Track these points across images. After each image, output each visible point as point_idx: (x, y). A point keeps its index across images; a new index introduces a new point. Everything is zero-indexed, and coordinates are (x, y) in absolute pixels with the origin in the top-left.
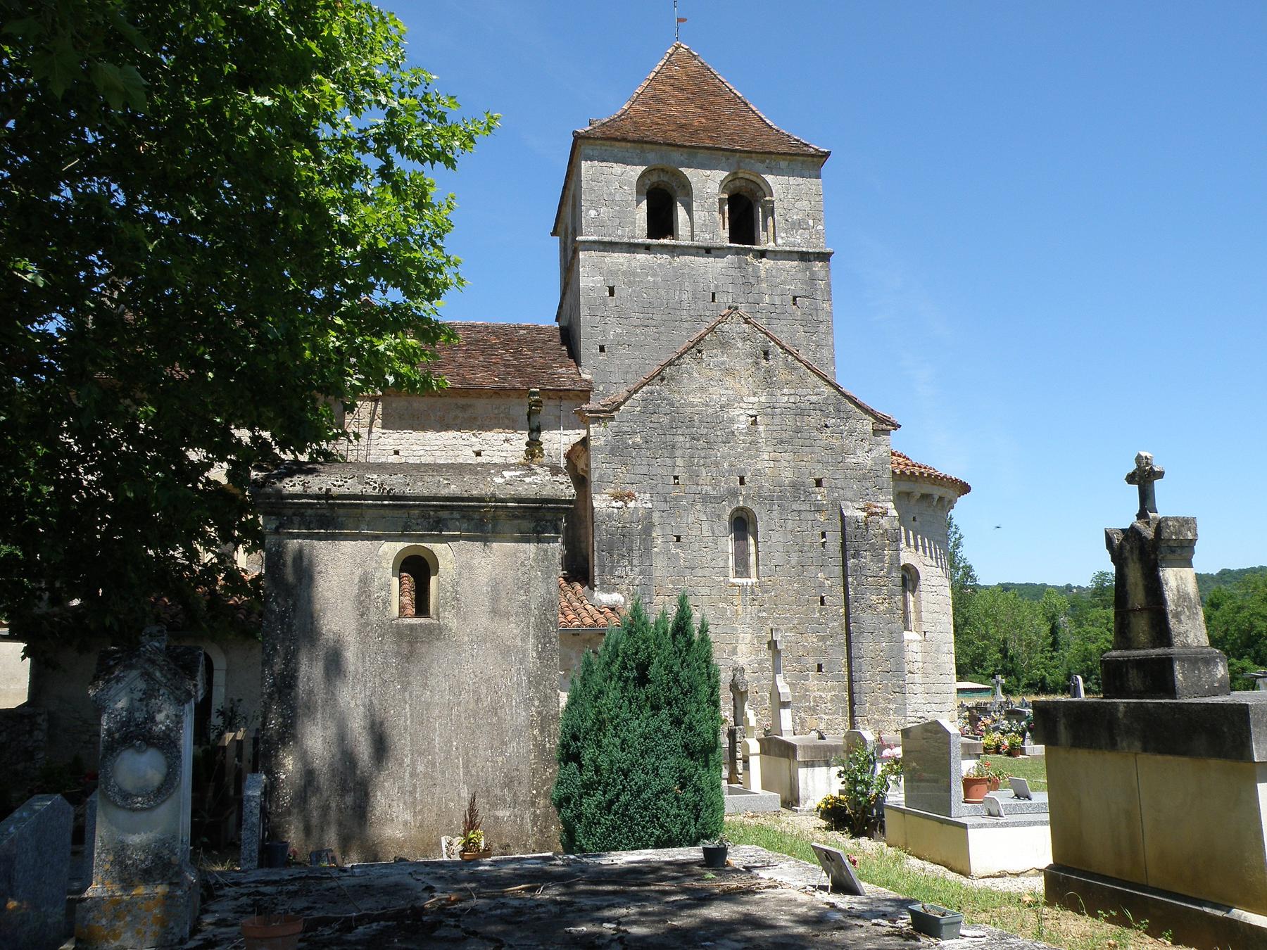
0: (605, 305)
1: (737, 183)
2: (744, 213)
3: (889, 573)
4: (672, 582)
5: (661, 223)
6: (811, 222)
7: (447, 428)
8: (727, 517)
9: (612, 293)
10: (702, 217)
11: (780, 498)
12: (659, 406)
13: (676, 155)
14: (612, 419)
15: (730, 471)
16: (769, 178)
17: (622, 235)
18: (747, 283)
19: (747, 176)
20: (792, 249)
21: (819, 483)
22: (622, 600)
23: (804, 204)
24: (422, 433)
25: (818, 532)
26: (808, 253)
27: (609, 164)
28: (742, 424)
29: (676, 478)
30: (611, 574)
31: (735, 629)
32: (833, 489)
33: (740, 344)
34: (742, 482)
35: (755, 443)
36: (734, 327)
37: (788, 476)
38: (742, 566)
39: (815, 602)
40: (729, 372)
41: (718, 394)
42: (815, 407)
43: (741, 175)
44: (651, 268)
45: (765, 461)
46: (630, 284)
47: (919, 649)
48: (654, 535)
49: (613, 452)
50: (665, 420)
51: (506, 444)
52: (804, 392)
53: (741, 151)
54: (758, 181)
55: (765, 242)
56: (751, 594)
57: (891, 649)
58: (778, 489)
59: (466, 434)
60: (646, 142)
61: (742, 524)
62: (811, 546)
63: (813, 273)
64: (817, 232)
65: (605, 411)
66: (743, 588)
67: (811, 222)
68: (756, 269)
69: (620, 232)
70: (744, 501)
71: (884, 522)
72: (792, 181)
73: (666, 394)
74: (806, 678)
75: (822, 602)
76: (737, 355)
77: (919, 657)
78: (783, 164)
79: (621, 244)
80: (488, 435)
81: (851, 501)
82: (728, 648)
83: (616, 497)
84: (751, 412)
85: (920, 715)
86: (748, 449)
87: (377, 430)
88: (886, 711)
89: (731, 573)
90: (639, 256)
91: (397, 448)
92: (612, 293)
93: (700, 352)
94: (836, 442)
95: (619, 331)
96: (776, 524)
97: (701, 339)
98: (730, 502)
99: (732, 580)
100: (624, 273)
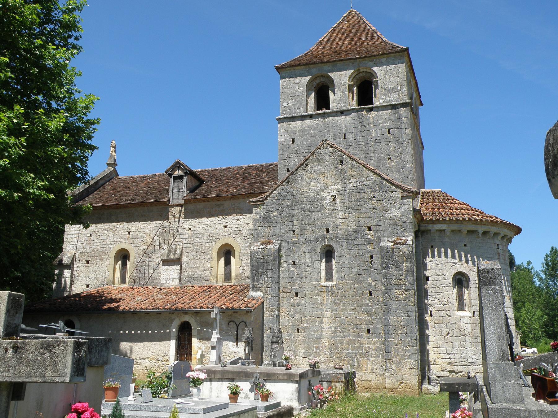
0: (290, 148)
1: (361, 75)
2: (365, 91)
3: (406, 276)
4: (291, 286)
5: (322, 101)
6: (399, 88)
7: (211, 215)
8: (319, 250)
9: (293, 142)
10: (341, 96)
11: (347, 238)
12: (286, 196)
13: (326, 67)
14: (264, 204)
15: (321, 226)
16: (376, 69)
17: (300, 112)
18: (363, 127)
19: (365, 70)
20: (387, 104)
21: (370, 229)
22: (262, 295)
23: (395, 79)
24: (201, 219)
25: (368, 256)
26: (396, 105)
27: (293, 79)
28: (328, 201)
29: (294, 231)
32: (377, 231)
33: (328, 159)
34: (328, 231)
36: (325, 151)
37: (352, 226)
38: (329, 276)
39: (366, 294)
40: (322, 174)
41: (316, 186)
42: (367, 187)
43: (361, 71)
44: (313, 126)
45: (340, 219)
46: (302, 136)
48: (282, 261)
49: (264, 221)
50: (289, 202)
51: (238, 222)
52: (362, 180)
53: (359, 58)
54: (371, 71)
55: (377, 102)
56: (331, 291)
57: (407, 321)
58: (346, 234)
59: (220, 218)
60: (311, 64)
61: (328, 254)
62: (364, 264)
63: (399, 115)
64: (403, 92)
65: (260, 201)
66: (327, 287)
67: (399, 88)
68: (368, 118)
69: (298, 111)
70: (328, 241)
71: (403, 248)
72: (388, 68)
73: (290, 189)
75: (371, 295)
76: (326, 165)
77: (469, 326)
78: (383, 60)
79: (298, 117)
80: (230, 218)
81: (388, 237)
82: (319, 320)
83: (263, 244)
84: (333, 194)
85: (469, 361)
86: (331, 213)
87: (182, 220)
88: (403, 357)
89: (323, 280)
90: (306, 121)
91: (190, 227)
92: (293, 142)
93: (307, 165)
94: (379, 205)
95: (296, 160)
96: (345, 253)
97: (308, 159)
98: (321, 242)
99: (323, 284)
100: (299, 131)
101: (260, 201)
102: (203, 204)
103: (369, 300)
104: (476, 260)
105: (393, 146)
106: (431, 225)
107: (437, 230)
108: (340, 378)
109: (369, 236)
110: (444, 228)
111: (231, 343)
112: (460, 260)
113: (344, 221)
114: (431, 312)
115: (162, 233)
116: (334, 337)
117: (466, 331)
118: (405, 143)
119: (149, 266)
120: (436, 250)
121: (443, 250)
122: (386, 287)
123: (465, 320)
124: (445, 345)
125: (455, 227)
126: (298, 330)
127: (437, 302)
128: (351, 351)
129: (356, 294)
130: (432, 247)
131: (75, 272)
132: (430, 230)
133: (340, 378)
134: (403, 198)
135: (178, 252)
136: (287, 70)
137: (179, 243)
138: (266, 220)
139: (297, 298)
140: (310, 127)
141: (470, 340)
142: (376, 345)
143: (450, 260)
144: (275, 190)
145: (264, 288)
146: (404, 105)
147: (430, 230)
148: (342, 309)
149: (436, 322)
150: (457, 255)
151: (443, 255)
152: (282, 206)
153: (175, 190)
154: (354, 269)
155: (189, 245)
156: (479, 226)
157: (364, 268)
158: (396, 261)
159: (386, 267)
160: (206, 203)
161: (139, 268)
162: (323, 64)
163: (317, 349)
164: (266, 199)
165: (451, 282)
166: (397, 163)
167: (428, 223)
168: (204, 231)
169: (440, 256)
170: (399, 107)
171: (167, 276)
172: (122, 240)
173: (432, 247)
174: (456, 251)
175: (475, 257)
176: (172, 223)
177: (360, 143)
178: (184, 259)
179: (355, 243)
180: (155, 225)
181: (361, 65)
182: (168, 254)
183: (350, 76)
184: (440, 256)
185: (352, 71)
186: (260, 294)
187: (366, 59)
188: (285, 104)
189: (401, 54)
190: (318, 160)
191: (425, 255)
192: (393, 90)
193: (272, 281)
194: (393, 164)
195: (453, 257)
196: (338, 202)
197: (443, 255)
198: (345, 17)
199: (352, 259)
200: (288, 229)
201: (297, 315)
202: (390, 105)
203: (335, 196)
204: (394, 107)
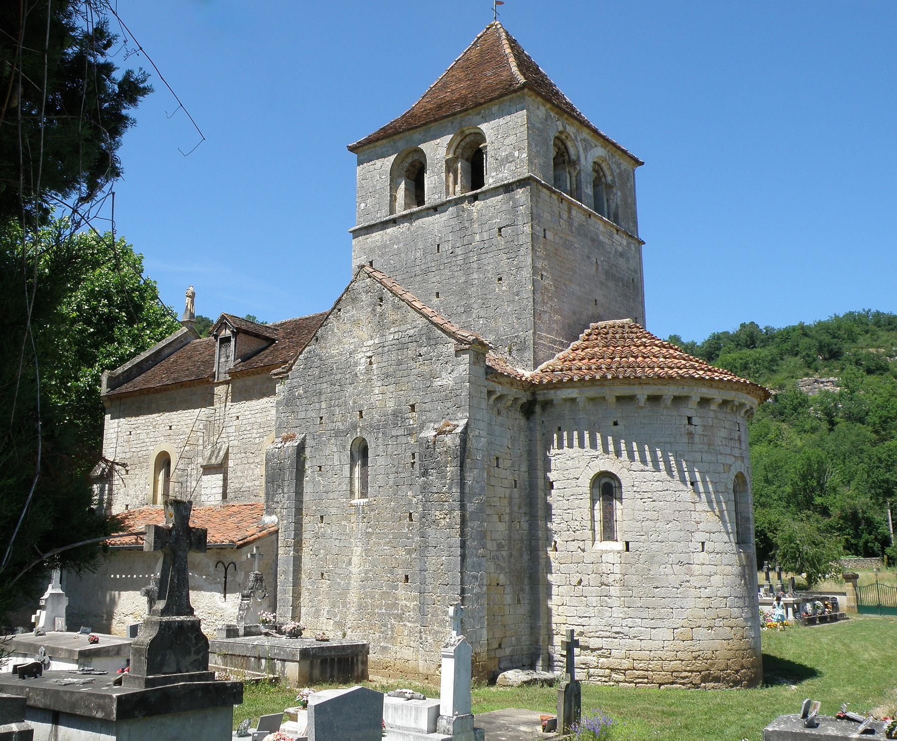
1: (468, 139)
3: (450, 489)
4: (315, 505)
6: (516, 154)
11: (384, 426)
13: (416, 135)
16: (484, 127)
23: (512, 139)
24: (250, 402)
27: (373, 162)
30: (272, 500)
31: (351, 543)
33: (364, 297)
35: (370, 380)
37: (391, 405)
40: (356, 322)
41: (349, 343)
42: (413, 339)
43: (467, 132)
45: (376, 396)
47: (618, 560)
48: (307, 466)
52: (403, 328)
65: (284, 373)
68: (470, 213)
69: (379, 215)
72: (501, 121)
74: (396, 588)
77: (617, 569)
78: (495, 109)
79: (377, 224)
82: (346, 559)
84: (369, 354)
85: (615, 629)
86: (366, 386)
90: (389, 231)
96: (380, 450)
97: (340, 300)
100: (379, 247)
101: (284, 373)
102: (253, 378)
103: (408, 527)
104: (635, 448)
105: (505, 256)
106: (552, 392)
107: (565, 400)
108: (294, 655)
109: (411, 422)
110: (574, 395)
111: (219, 594)
112: (606, 451)
113: (381, 398)
114: (556, 542)
115: (206, 425)
116: (364, 587)
117: (612, 578)
118: (523, 251)
119: (191, 475)
120: (565, 434)
121: (575, 433)
122: (423, 506)
123: (610, 558)
124: (575, 601)
125: (591, 392)
126: (322, 574)
127: (564, 525)
128: (384, 611)
129: (393, 517)
130: (560, 429)
131: (114, 488)
132: (552, 400)
133: (294, 655)
134: (458, 353)
135: (222, 453)
136: (365, 150)
137: (225, 440)
138: (289, 402)
139: (323, 525)
140: (394, 240)
141: (618, 594)
142: (415, 603)
143: (588, 451)
144: (301, 353)
145: (279, 510)
146: (522, 183)
147: (552, 400)
148: (375, 543)
149: (562, 561)
150: (599, 441)
151: (576, 442)
152: (308, 378)
153: (223, 360)
154: (391, 476)
155: (236, 443)
156: (635, 387)
157: (402, 475)
158: (438, 462)
159: (425, 474)
160: (257, 376)
161: (180, 480)
162: (411, 132)
163: (343, 607)
164: (290, 369)
165: (587, 490)
166: (511, 287)
167: (547, 389)
168: (253, 420)
169: (571, 446)
170: (515, 187)
171: (208, 491)
172: (162, 438)
173: (560, 429)
174: (598, 435)
175: (634, 444)
176: (218, 410)
177: (459, 258)
178: (231, 463)
179: (393, 434)
180: (204, 412)
181: (463, 123)
182: (210, 458)
183: (450, 145)
184: (571, 446)
185: (448, 138)
186: (274, 518)
187: (470, 111)
188: (363, 205)
189: (519, 93)
190: (353, 300)
191: (547, 446)
192: (508, 159)
193: (288, 499)
194: (504, 288)
195: (593, 446)
196: (374, 366)
197: (576, 442)
198: (479, 38)
199: (389, 460)
200: (314, 415)
201: (322, 551)
202: (501, 186)
203: (371, 357)
204: (508, 188)
